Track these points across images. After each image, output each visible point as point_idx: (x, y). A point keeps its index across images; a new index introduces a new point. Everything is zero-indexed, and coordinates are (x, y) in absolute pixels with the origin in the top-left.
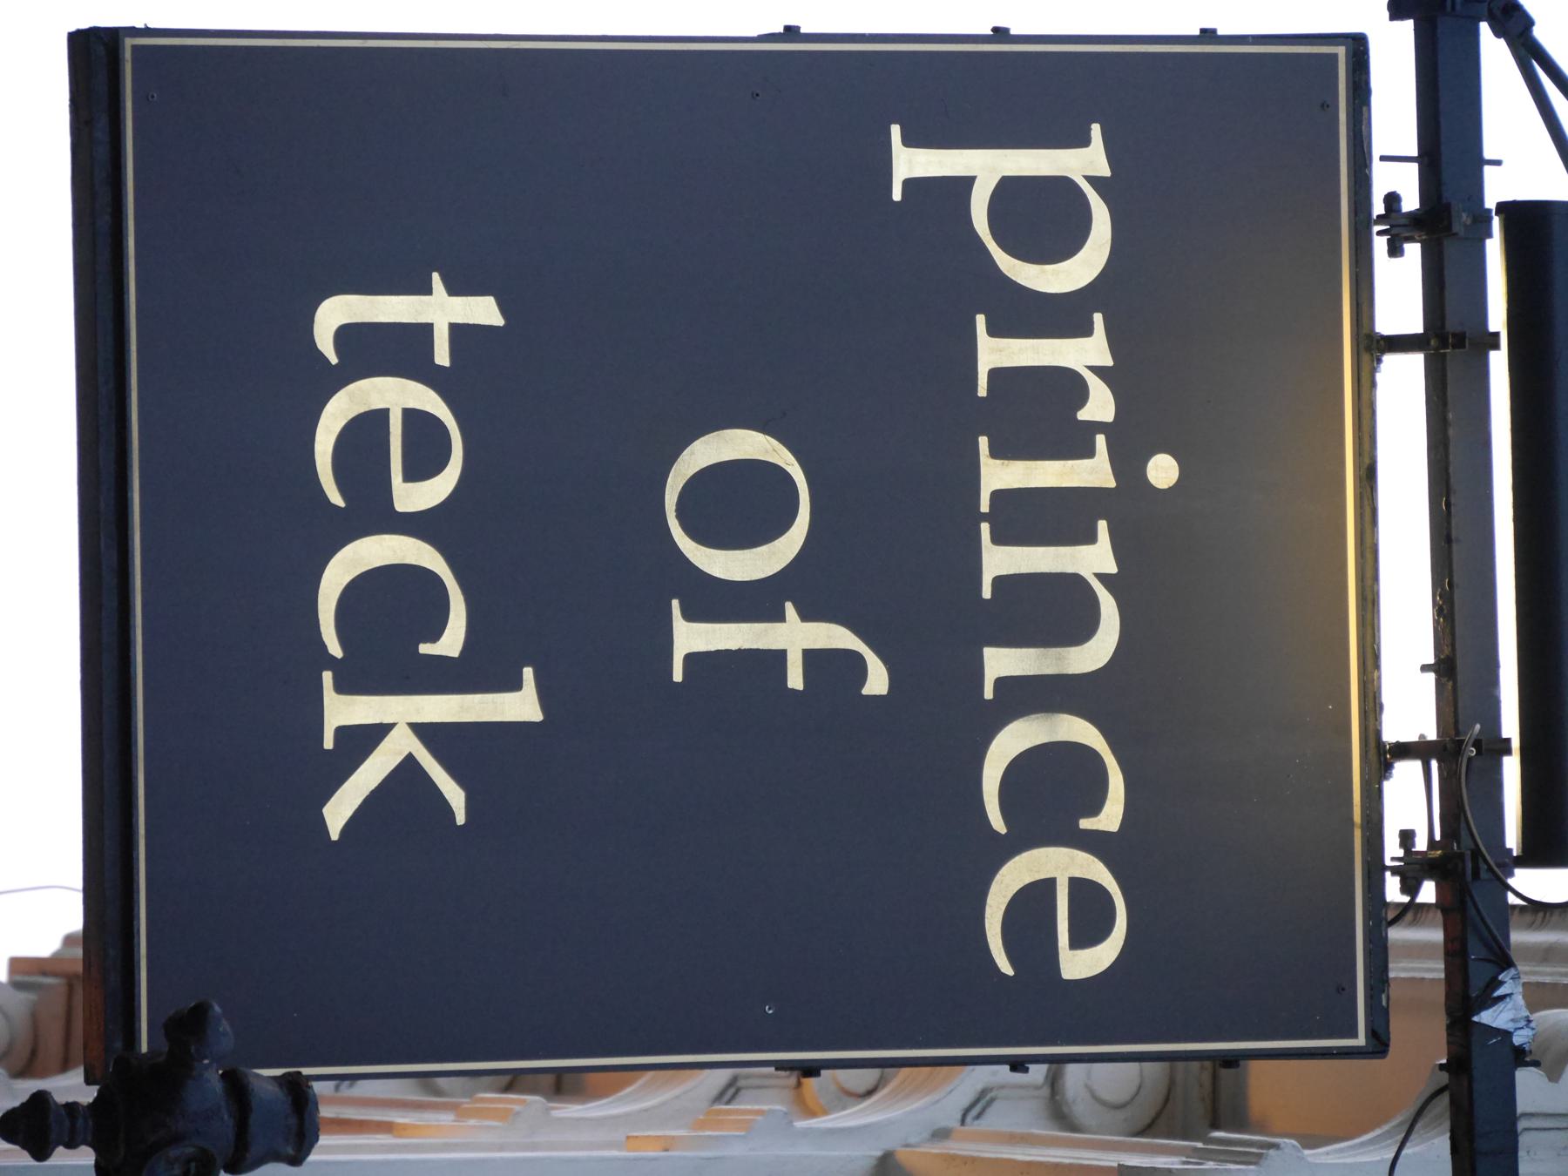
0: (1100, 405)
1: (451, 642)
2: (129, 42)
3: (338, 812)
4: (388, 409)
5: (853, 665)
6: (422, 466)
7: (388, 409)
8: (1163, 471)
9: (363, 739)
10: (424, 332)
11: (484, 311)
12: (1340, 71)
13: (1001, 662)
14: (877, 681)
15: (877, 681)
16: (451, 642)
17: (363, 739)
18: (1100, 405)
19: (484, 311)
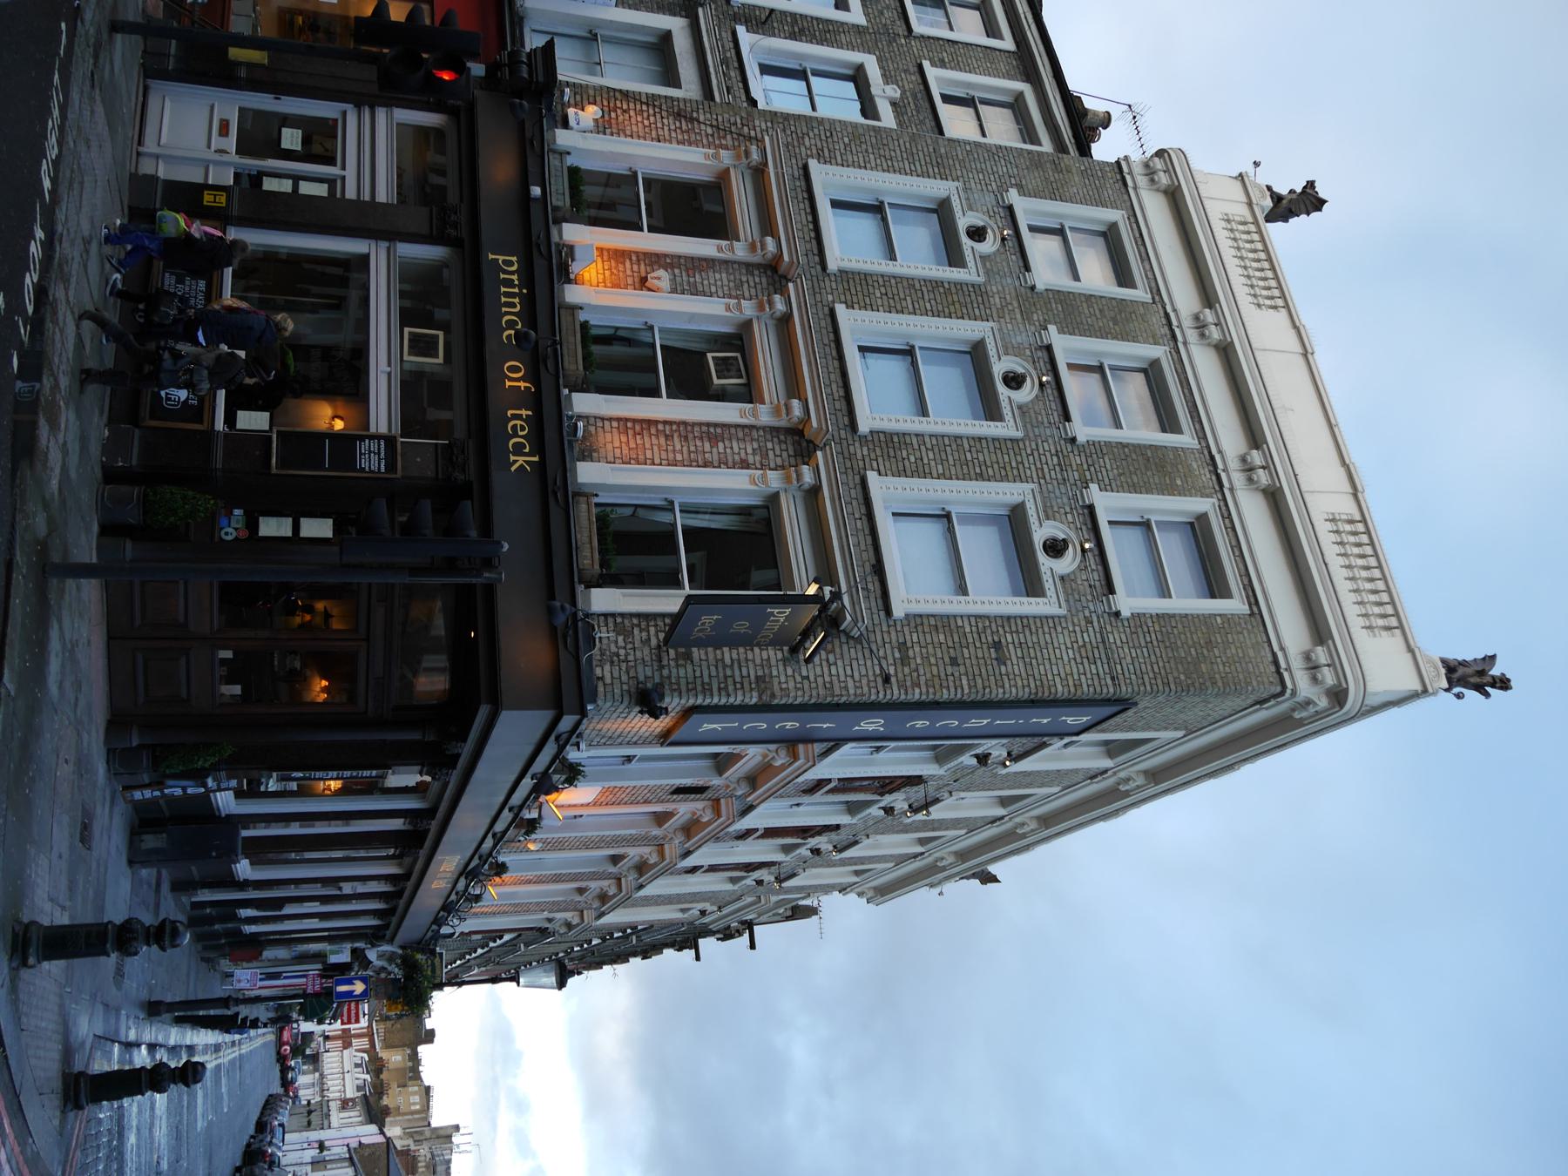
1: (527, 450)
16: (527, 450)
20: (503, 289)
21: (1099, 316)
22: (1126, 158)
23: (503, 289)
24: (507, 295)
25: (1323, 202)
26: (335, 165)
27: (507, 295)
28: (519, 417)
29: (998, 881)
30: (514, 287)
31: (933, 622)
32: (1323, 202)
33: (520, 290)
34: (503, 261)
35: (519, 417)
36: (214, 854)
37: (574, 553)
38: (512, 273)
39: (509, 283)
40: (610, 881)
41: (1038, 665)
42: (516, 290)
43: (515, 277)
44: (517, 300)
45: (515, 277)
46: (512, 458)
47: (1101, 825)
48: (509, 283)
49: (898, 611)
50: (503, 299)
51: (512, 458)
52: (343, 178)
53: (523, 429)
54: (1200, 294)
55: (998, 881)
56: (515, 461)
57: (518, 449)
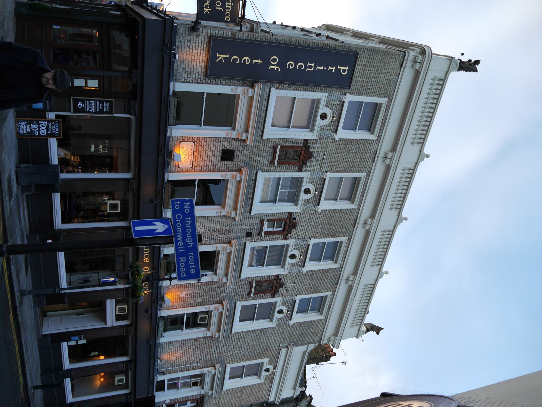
1: (209, 7)
16: (209, 7)
22: (455, 58)
24: (228, 5)
25: (379, 334)
27: (228, 5)
30: (230, 3)
31: (275, 141)
32: (379, 334)
33: (231, 4)
40: (211, 368)
41: (358, 69)
42: (230, 4)
44: (230, 7)
46: (205, 9)
47: (413, 184)
49: (265, 138)
51: (205, 9)
54: (343, 306)
56: (205, 10)
57: (207, 6)
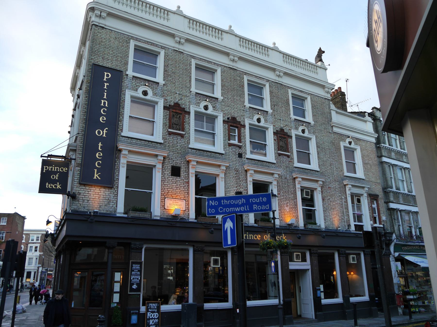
0: (52, 167)
1: (56, 185)
2: (300, 261)
3: (60, 188)
4: (39, 192)
5: (106, 129)
6: (51, 185)
7: (39, 192)
8: (54, 166)
9: (96, 177)
10: (101, 146)
11: (47, 183)
12: (16, 283)
13: (58, 170)
14: (107, 129)
15: (107, 129)
16: (56, 185)
17: (59, 187)
18: (52, 167)
19: (47, 183)
20: (248, 238)
21: (164, 181)
23: (248, 238)
24: (249, 237)
26: (356, 222)
27: (249, 237)
28: (48, 186)
29: (320, 48)
34: (45, 169)
35: (48, 186)
36: (247, 233)
37: (146, 219)
38: (49, 168)
39: (52, 169)
43: (50, 167)
45: (50, 167)
48: (52, 169)
50: (250, 238)
52: (355, 221)
53: (51, 185)
55: (320, 48)
